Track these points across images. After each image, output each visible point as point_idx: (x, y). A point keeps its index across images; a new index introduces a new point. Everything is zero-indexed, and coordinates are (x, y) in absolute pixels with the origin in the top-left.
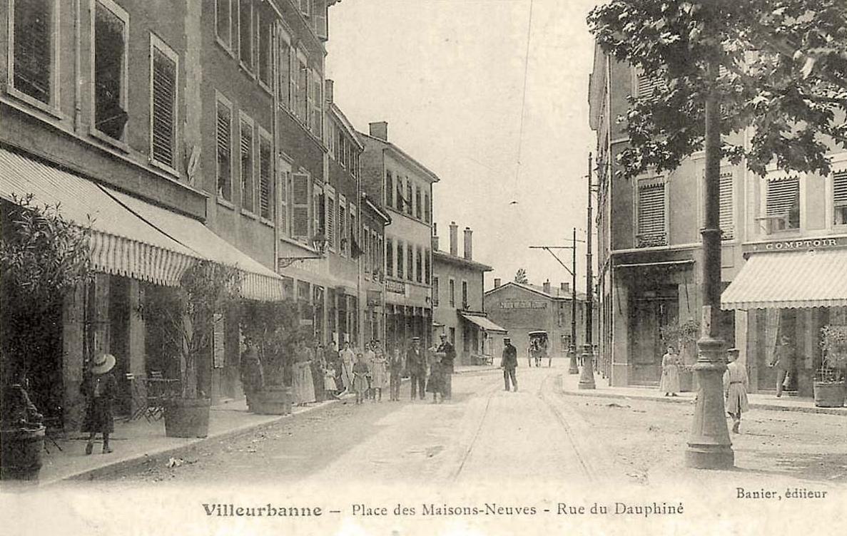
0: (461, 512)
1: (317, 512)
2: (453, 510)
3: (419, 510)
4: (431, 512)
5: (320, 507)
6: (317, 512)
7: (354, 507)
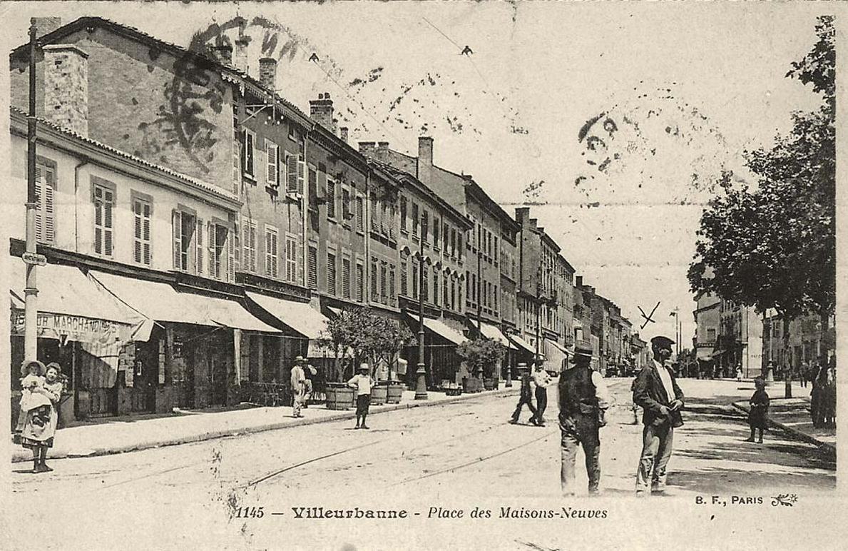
0: (537, 514)
1: (402, 514)
2: (530, 513)
3: (496, 513)
4: (506, 515)
5: (406, 510)
6: (402, 514)
7: (431, 508)
